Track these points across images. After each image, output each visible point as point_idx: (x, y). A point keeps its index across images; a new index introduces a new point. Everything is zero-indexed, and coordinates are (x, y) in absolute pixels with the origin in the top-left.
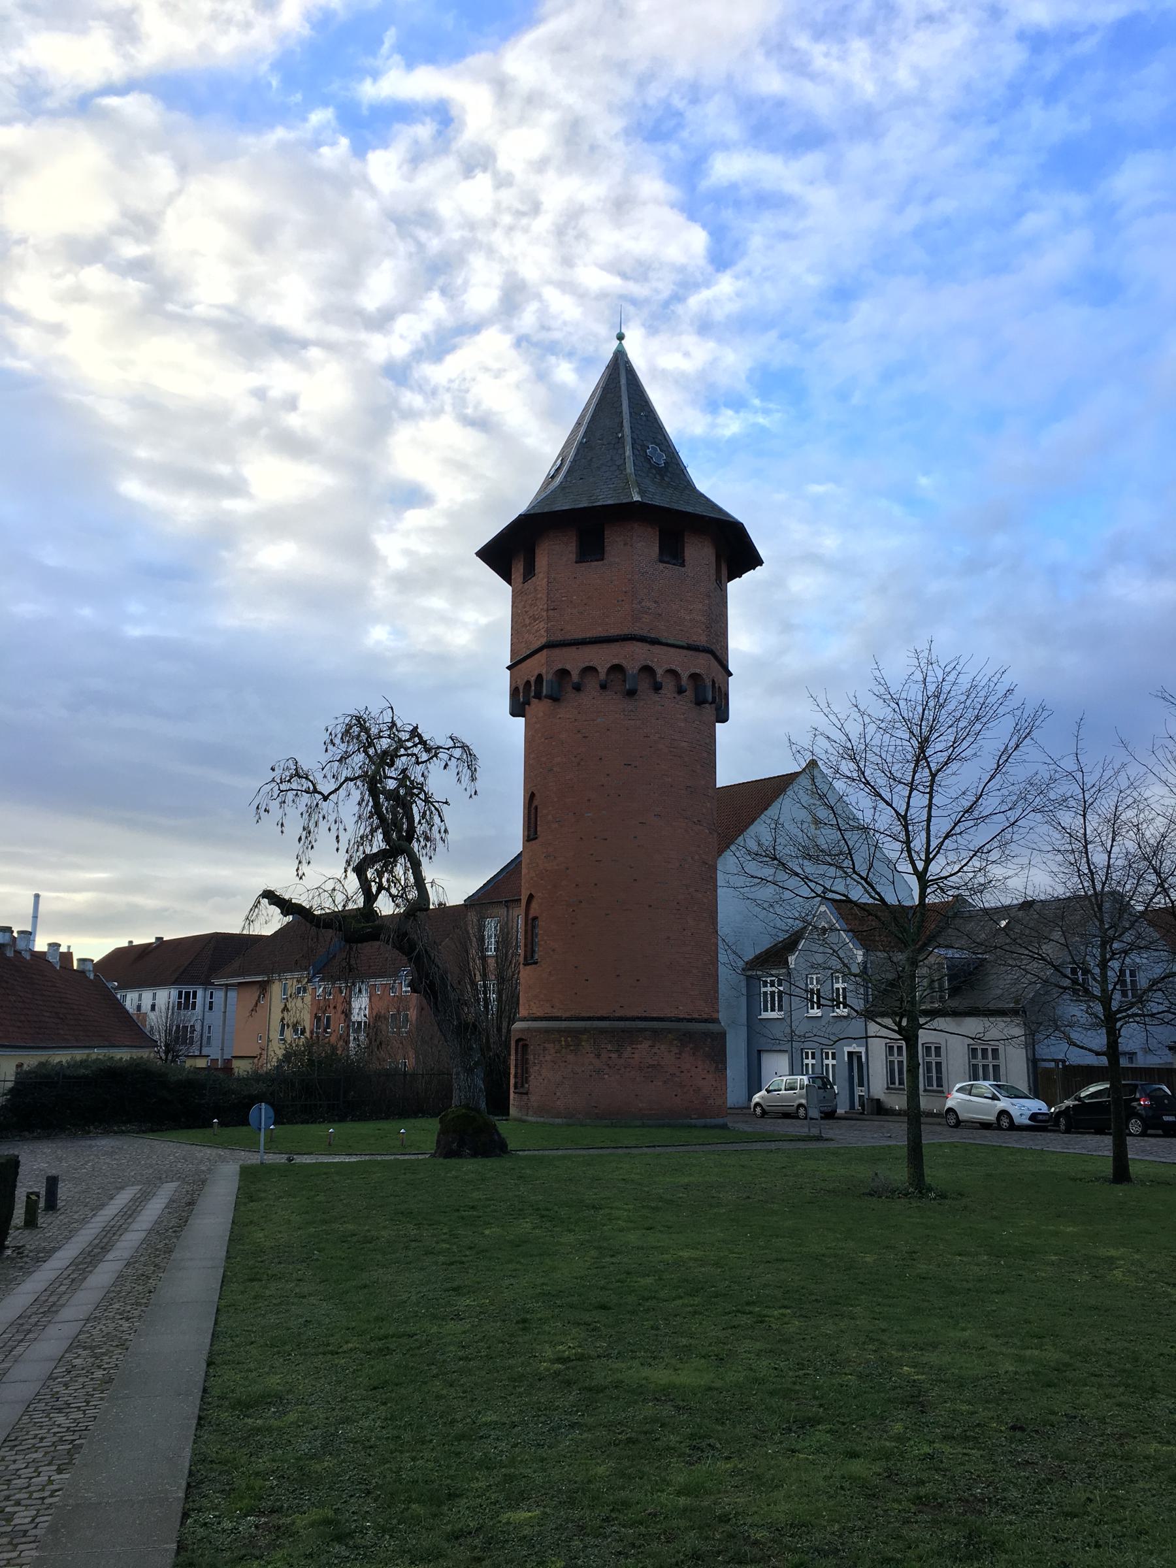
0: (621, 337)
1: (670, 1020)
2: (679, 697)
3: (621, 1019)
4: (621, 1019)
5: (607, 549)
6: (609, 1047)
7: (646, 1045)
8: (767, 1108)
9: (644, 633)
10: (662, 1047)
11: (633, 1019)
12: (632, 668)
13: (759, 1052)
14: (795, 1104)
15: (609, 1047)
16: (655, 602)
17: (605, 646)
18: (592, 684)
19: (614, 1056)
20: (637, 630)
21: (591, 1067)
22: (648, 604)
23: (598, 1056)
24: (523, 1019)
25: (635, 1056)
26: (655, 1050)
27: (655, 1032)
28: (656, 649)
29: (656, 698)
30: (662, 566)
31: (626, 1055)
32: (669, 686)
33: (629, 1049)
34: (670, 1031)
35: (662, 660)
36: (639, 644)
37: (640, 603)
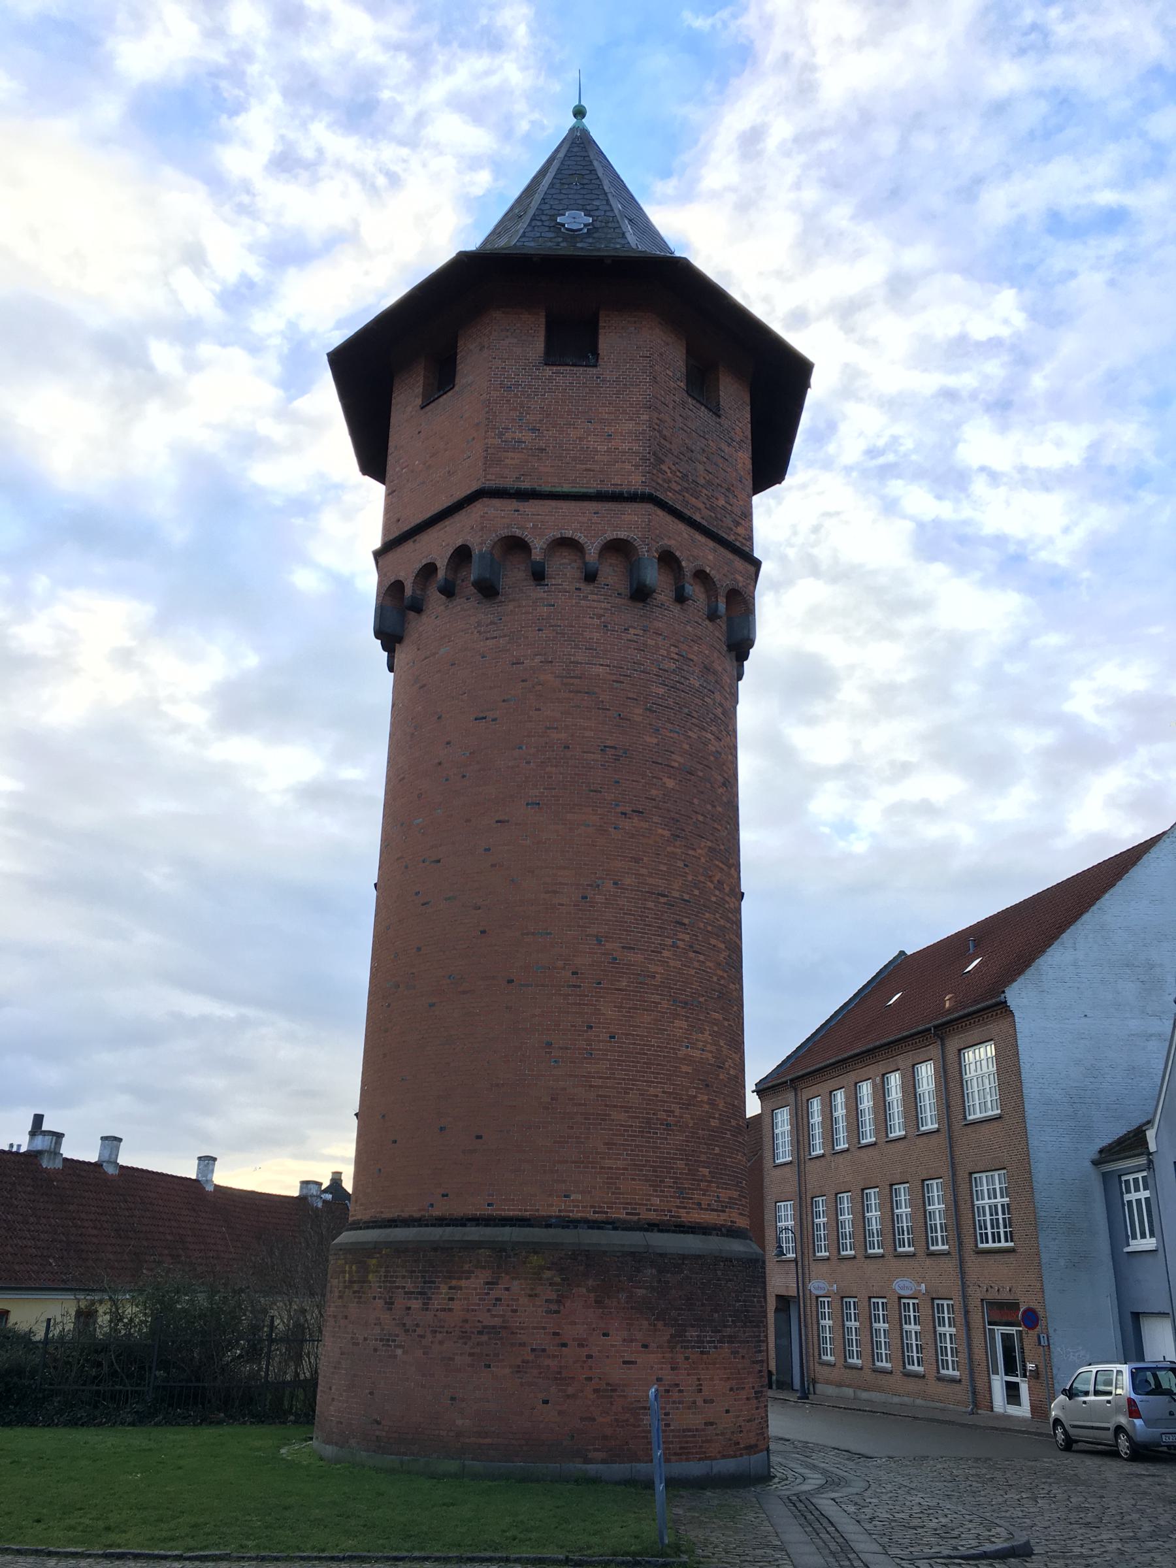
0: (579, 113)
1: (546, 1223)
2: (587, 588)
3: (441, 1222)
4: (441, 1222)
5: (459, 368)
6: (409, 1286)
7: (475, 1283)
8: (1071, 1431)
9: (509, 483)
10: (516, 1285)
11: (463, 1222)
12: (480, 544)
13: (1136, 1316)
14: (1111, 1425)
15: (409, 1286)
16: (534, 430)
17: (447, 522)
18: (435, 598)
19: (416, 1304)
20: (494, 482)
21: (377, 1330)
22: (518, 435)
23: (389, 1304)
24: (357, 1226)
25: (456, 1305)
26: (498, 1292)
27: (500, 1250)
28: (532, 508)
29: (539, 593)
30: (548, 371)
31: (435, 1304)
32: (564, 570)
33: (444, 1289)
34: (535, 1248)
35: (540, 524)
36: (496, 502)
37: (501, 435)
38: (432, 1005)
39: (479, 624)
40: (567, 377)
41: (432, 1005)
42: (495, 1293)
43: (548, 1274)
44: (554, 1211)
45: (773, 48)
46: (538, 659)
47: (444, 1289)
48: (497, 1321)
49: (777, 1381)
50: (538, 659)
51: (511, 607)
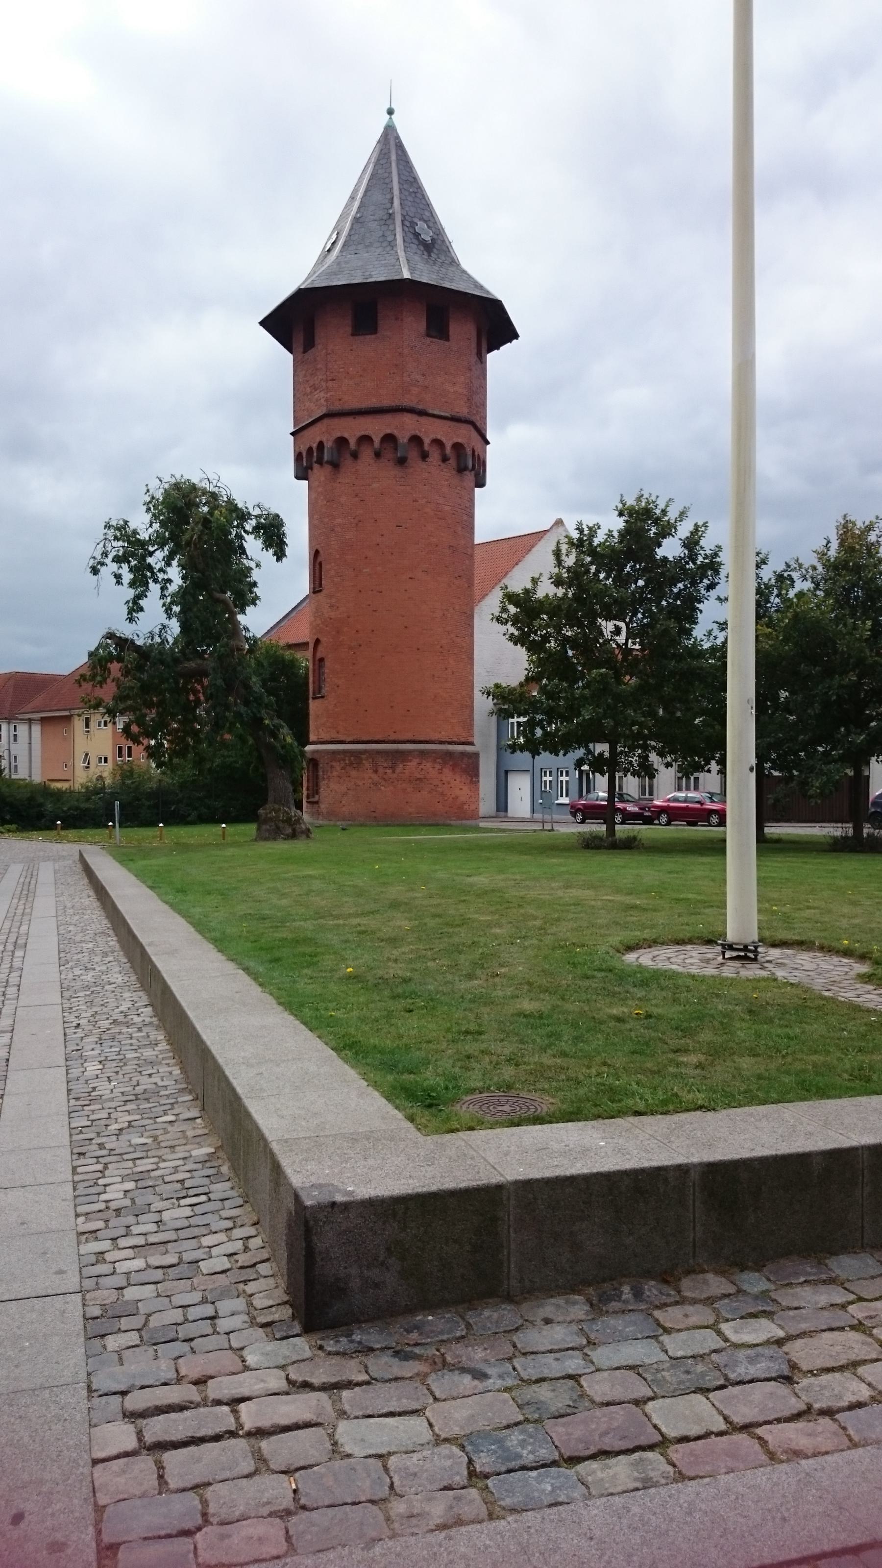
2: (443, 465)
6: (385, 765)
7: (414, 763)
18: (367, 454)
19: (389, 771)
21: (370, 781)
25: (406, 771)
32: (435, 455)
36: (409, 415)
38: (382, 656)
39: (396, 477)
40: (437, 345)
41: (382, 656)
42: (421, 767)
43: (438, 760)
44: (436, 738)
45: (812, 939)
46: (425, 500)
47: (401, 766)
48: (421, 777)
49: (702, 747)
50: (425, 500)
51: (411, 470)
